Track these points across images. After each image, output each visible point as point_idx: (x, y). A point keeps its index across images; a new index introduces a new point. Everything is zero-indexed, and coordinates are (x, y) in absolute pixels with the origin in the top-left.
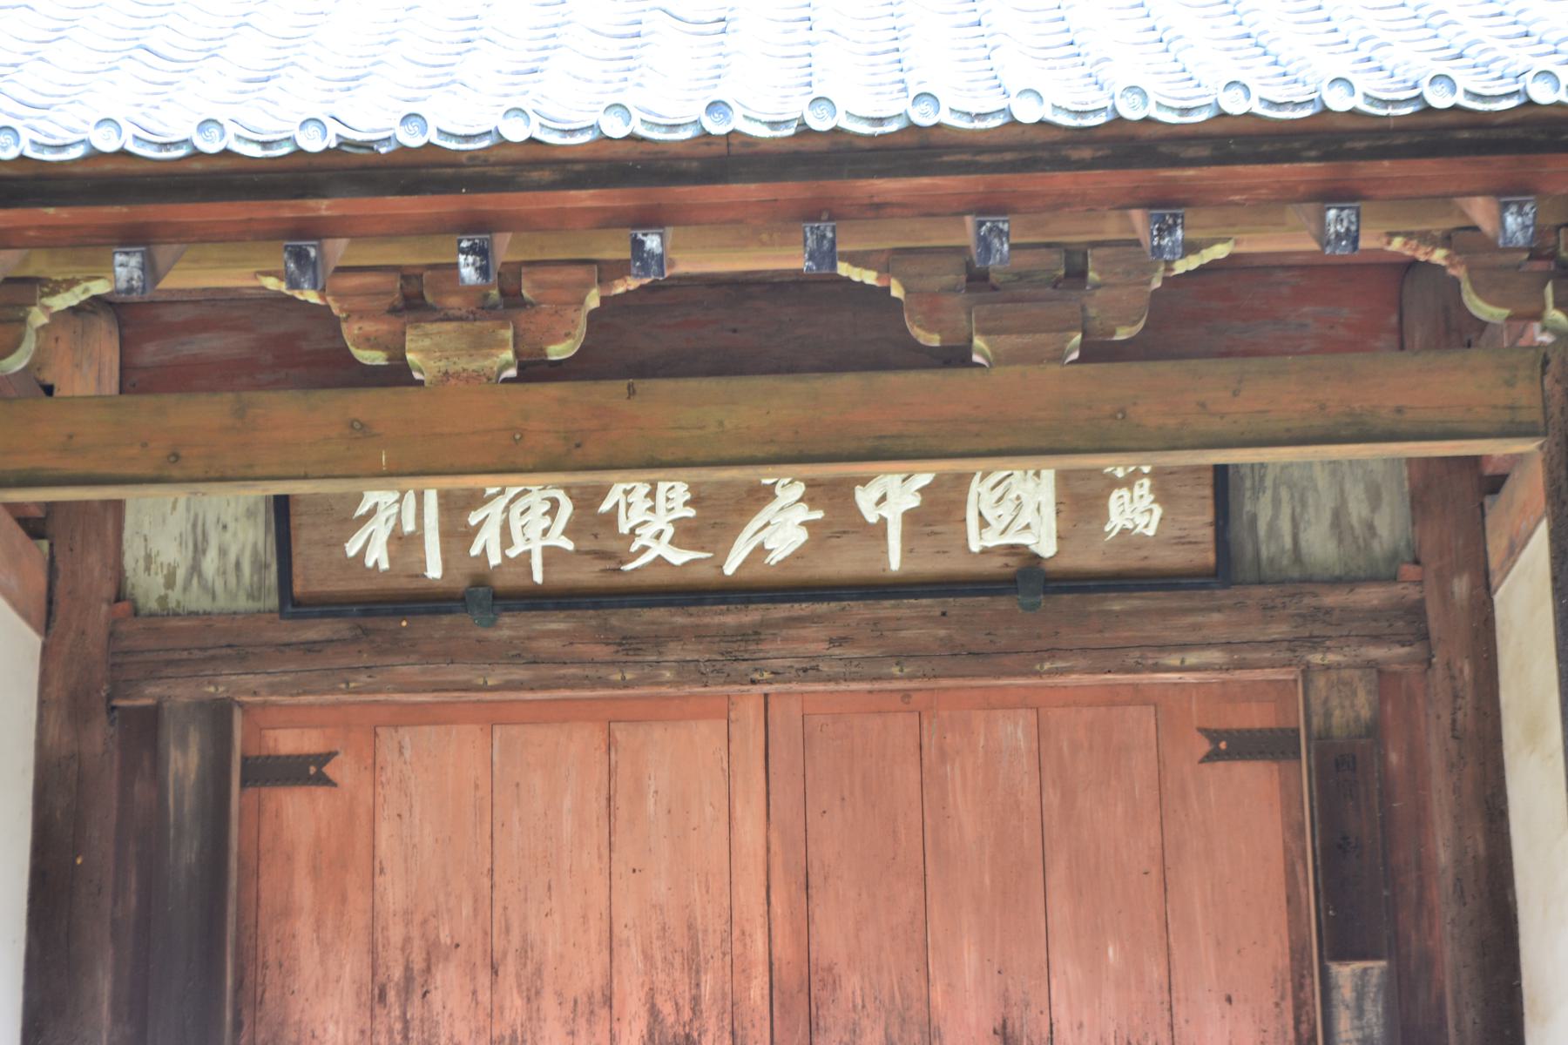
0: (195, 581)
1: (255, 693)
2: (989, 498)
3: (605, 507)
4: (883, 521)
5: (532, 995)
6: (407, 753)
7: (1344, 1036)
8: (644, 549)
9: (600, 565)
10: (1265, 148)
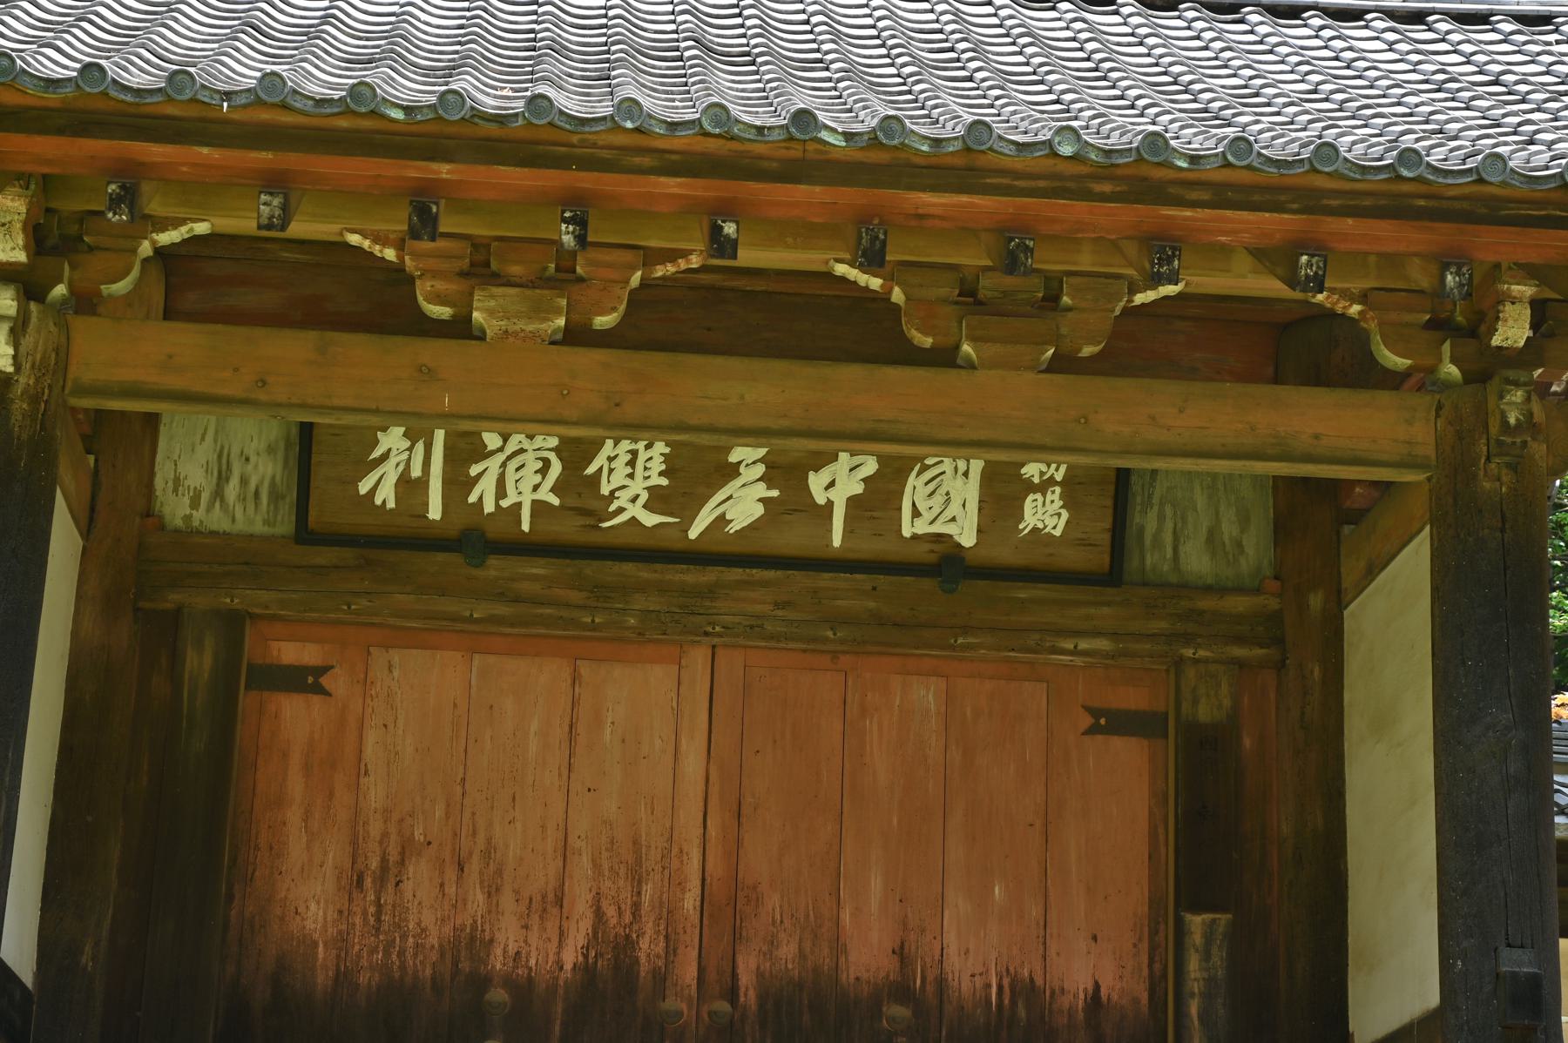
0: (217, 504)
1: (267, 607)
2: (923, 491)
3: (591, 470)
4: (830, 504)
5: (493, 891)
6: (396, 673)
7: (1192, 976)
8: (621, 510)
9: (581, 521)
10: (1256, 198)
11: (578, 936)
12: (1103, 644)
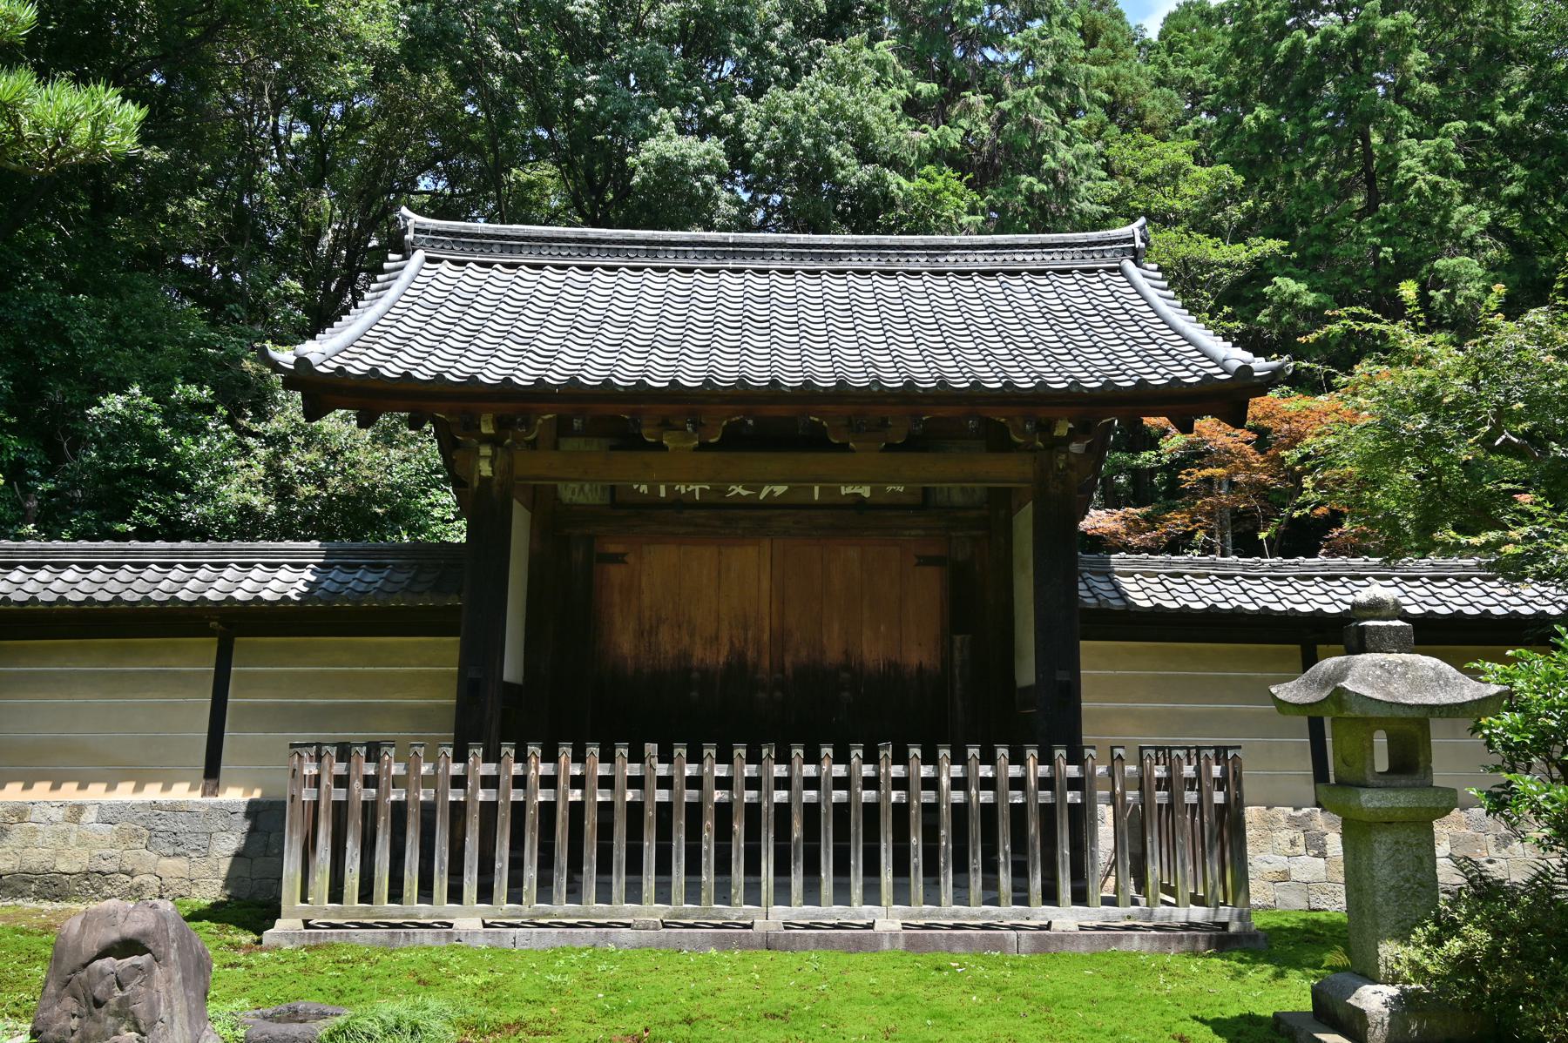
11: (725, 651)
12: (921, 532)
